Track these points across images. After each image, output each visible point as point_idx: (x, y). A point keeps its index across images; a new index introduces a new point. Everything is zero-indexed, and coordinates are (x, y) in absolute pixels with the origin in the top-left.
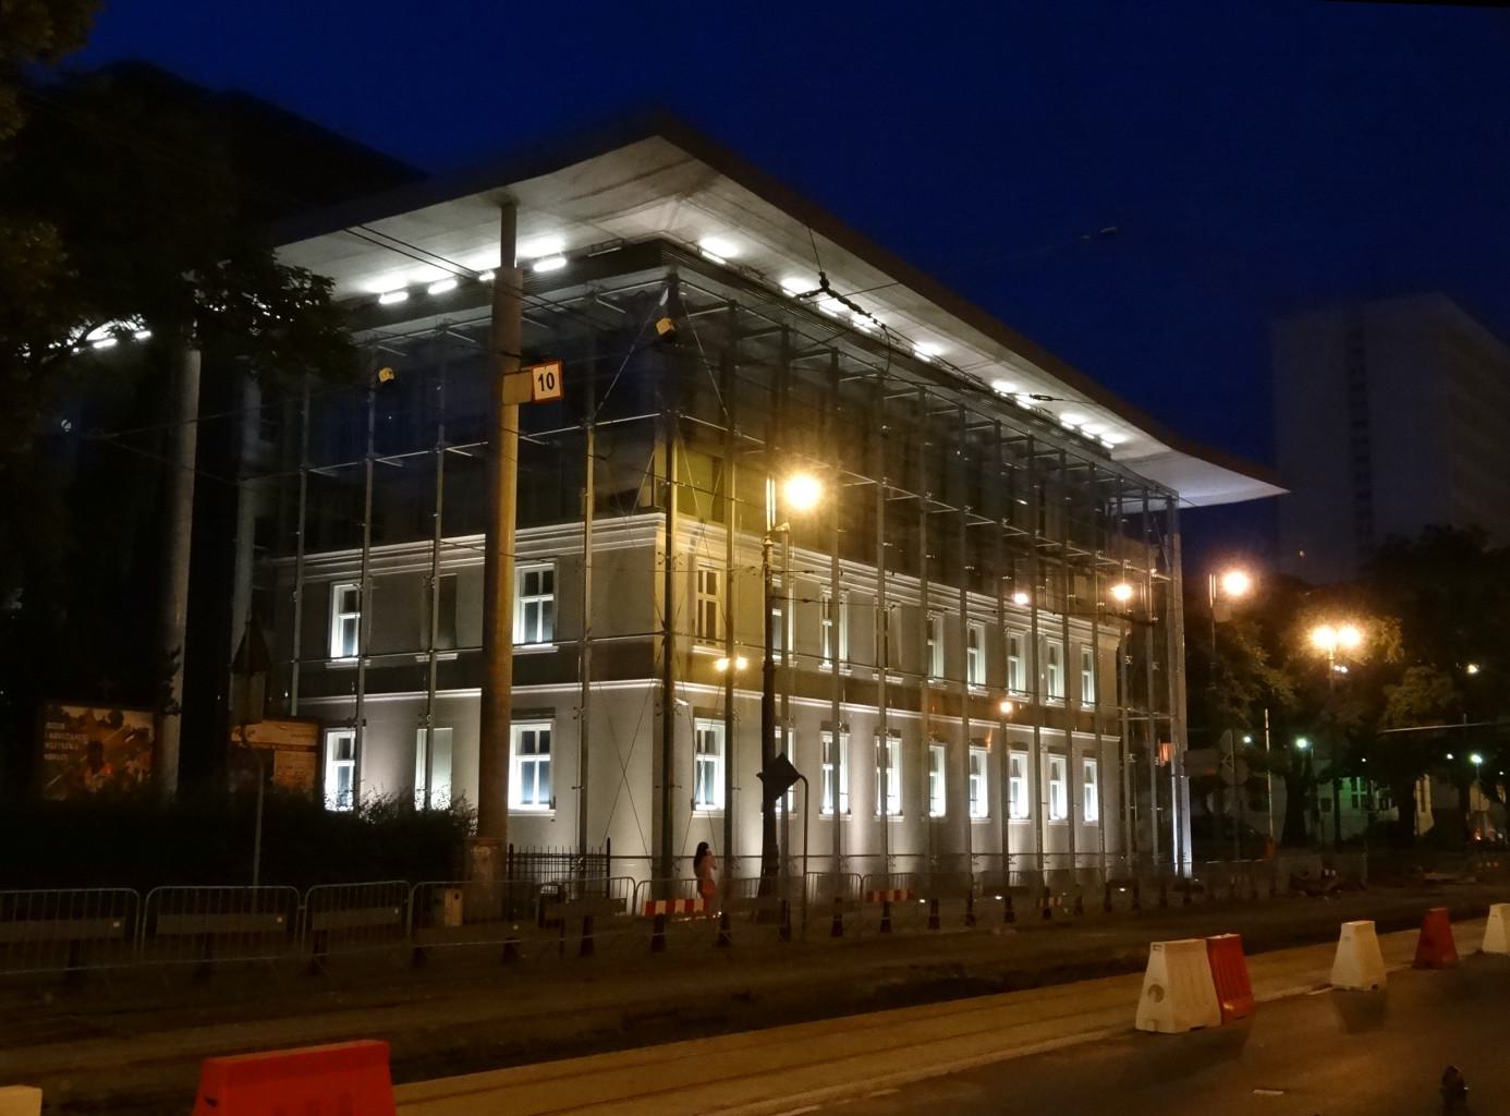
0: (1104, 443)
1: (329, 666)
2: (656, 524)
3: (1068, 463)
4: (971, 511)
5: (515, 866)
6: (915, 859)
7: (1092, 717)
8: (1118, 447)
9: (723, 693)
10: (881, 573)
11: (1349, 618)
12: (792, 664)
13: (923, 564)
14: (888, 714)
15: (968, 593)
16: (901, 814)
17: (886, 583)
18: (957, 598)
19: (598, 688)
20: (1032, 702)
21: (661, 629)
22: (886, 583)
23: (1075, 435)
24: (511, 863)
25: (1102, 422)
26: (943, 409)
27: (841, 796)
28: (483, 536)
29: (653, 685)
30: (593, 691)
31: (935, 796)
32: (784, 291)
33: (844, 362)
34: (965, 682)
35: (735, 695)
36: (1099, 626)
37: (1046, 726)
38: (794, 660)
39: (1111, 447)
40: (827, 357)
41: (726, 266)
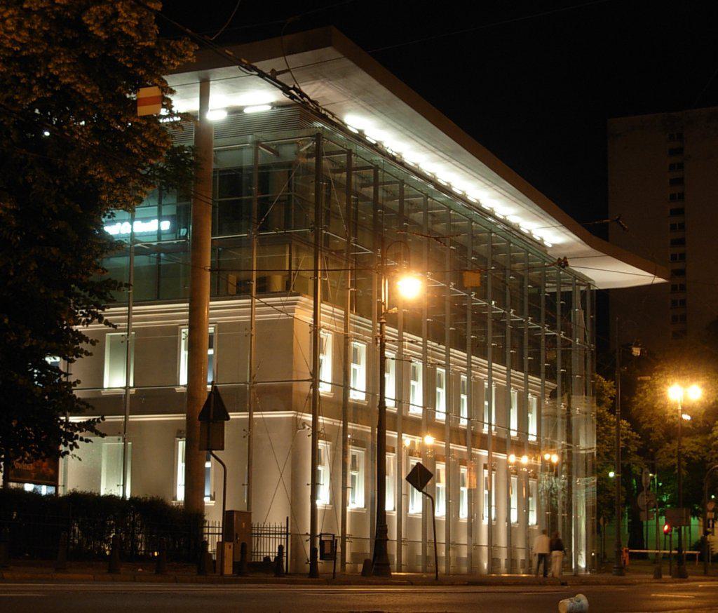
0: (545, 243)
1: (104, 393)
2: (295, 304)
3: (354, 166)
4: (454, 287)
5: (274, 536)
6: (524, 550)
7: (465, 432)
8: (555, 246)
9: (342, 425)
10: (508, 371)
11: (683, 368)
12: (494, 433)
13: (543, 370)
14: (451, 447)
15: (452, 350)
16: (537, 524)
17: (451, 358)
18: (486, 368)
19: (261, 416)
20: (370, 406)
21: (309, 377)
22: (451, 358)
23: (360, 138)
24: (267, 534)
25: (534, 220)
26: (412, 197)
27: (512, 510)
28: (188, 305)
29: (292, 415)
30: (256, 418)
31: (321, 483)
32: (367, 138)
33: (355, 161)
34: (527, 434)
35: (349, 427)
36: (350, 315)
37: (354, 422)
38: (495, 430)
39: (550, 246)
40: (370, 173)
41: (447, 187)
